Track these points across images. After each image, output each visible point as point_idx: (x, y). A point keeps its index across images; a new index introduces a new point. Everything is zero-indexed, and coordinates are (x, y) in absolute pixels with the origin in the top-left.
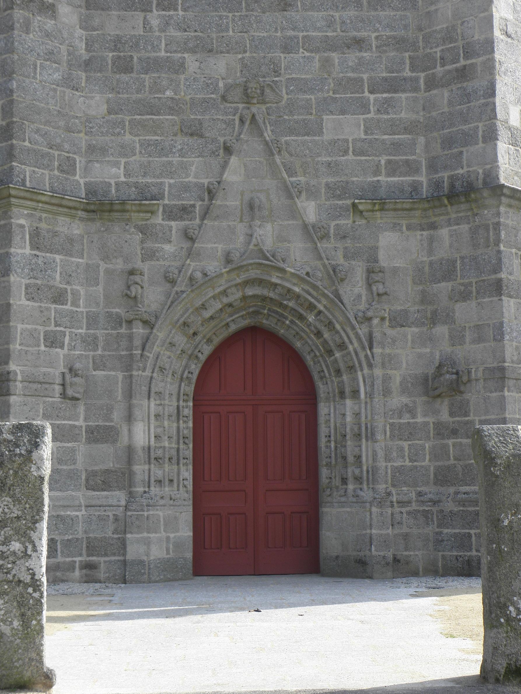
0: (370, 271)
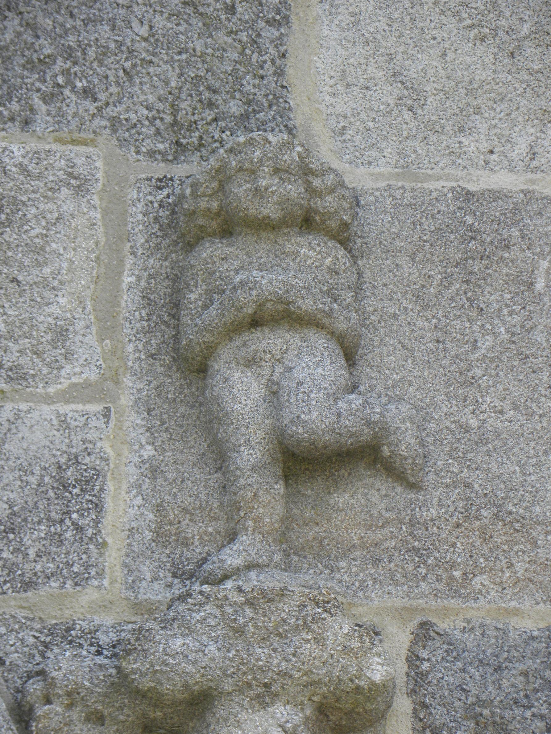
0: (192, 226)
